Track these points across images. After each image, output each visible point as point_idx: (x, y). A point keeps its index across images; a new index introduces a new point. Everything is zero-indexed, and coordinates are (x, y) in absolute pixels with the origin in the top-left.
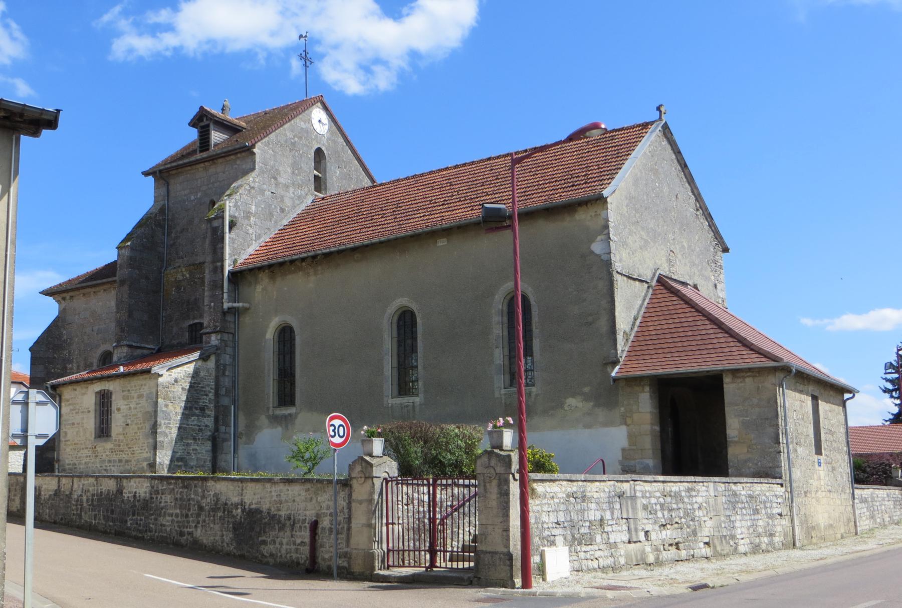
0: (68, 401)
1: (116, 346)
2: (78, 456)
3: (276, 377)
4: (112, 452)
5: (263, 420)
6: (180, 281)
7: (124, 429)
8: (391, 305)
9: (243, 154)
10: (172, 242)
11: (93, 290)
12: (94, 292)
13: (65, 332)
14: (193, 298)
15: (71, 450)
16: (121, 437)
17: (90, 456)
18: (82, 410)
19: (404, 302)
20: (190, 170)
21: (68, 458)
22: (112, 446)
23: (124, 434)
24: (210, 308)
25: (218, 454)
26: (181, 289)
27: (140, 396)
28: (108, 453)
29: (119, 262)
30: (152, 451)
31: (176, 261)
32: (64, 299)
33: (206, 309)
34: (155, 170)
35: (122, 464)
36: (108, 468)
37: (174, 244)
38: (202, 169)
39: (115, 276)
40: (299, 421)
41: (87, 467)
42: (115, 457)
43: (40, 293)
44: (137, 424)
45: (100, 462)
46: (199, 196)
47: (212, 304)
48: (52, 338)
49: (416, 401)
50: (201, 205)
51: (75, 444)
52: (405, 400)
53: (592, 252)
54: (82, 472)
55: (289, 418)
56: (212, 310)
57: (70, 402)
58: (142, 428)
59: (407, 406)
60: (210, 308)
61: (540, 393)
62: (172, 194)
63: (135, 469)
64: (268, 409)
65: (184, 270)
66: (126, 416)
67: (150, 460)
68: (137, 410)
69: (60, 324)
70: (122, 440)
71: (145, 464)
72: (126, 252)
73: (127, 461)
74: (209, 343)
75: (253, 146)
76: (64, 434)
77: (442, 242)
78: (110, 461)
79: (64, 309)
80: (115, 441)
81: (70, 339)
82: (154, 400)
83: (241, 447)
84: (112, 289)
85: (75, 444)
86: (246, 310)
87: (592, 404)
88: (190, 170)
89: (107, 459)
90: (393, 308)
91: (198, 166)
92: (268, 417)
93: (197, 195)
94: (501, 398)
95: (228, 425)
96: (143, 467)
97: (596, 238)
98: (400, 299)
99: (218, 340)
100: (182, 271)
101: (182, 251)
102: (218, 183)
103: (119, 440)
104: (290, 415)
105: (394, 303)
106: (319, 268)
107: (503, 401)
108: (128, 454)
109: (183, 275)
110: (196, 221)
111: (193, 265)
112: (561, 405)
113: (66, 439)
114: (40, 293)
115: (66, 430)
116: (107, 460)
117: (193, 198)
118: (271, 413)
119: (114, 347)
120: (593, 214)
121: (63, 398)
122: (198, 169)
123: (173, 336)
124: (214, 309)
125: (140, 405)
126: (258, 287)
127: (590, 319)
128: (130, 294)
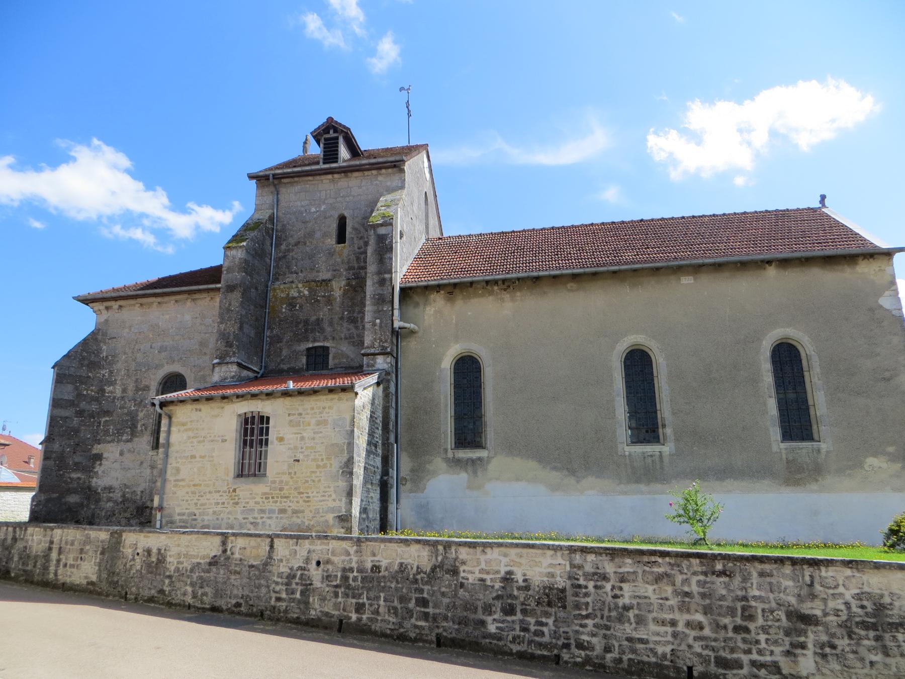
0: (183, 424)
1: (219, 364)
2: (199, 502)
3: (453, 414)
4: (266, 498)
5: (438, 463)
6: (294, 298)
7: (289, 466)
8: (622, 341)
9: (390, 170)
10: (280, 255)
11: (159, 299)
12: (159, 303)
13: (104, 347)
14: (313, 318)
15: (187, 493)
16: (285, 478)
17: (223, 503)
18: (212, 438)
19: (639, 340)
20: (310, 181)
21: (179, 505)
22: (267, 490)
23: (290, 474)
24: (374, 325)
25: (389, 504)
26: (296, 306)
27: (322, 423)
28: (258, 499)
29: (226, 264)
30: (344, 499)
31: (287, 276)
32: (107, 308)
33: (368, 326)
34: (267, 173)
35: (287, 515)
36: (259, 521)
37: (284, 257)
38: (328, 181)
39: (219, 282)
40: (493, 466)
41: (218, 519)
42: (270, 505)
43: (74, 298)
44: (314, 460)
45: (243, 512)
46: (322, 209)
47: (378, 321)
48: (87, 353)
49: (663, 450)
50: (325, 218)
51: (194, 485)
52: (649, 449)
53: (881, 307)
54: (309, 529)
55: (479, 462)
56: (377, 328)
57: (189, 426)
58: (325, 466)
59: (651, 456)
60: (374, 325)
61: (832, 449)
62: (283, 204)
63: (312, 523)
64: (446, 450)
65: (300, 285)
66: (296, 448)
67: (340, 512)
68: (315, 441)
69: (100, 337)
70: (287, 483)
71: (330, 517)
72: (239, 254)
73: (295, 512)
74: (373, 366)
75: (403, 161)
76: (174, 471)
77: (771, 272)
78: (262, 511)
79: (107, 321)
80: (274, 482)
81: (112, 356)
82: (348, 428)
83: (403, 496)
84: (190, 300)
85: (194, 485)
86: (412, 332)
87: (900, 465)
88: (310, 181)
89: (258, 507)
90: (625, 345)
91: (323, 177)
92: (447, 460)
93: (320, 207)
94: (781, 452)
95: (393, 469)
96: (327, 521)
97: (884, 292)
98: (634, 336)
99: (388, 363)
100: (297, 287)
101: (296, 266)
102: (351, 198)
103: (281, 482)
104: (480, 459)
105: (625, 339)
106: (518, 294)
107: (784, 456)
108: (298, 502)
109: (299, 292)
110: (318, 235)
111: (315, 281)
112: (861, 465)
113: (178, 478)
114: (73, 298)
115: (178, 465)
116: (256, 508)
117: (313, 210)
118: (450, 454)
119: (214, 364)
120: (877, 269)
121: (174, 419)
122: (322, 180)
123: (283, 360)
124: (381, 327)
125: (320, 435)
126: (428, 309)
127: (887, 374)
128: (242, 302)
